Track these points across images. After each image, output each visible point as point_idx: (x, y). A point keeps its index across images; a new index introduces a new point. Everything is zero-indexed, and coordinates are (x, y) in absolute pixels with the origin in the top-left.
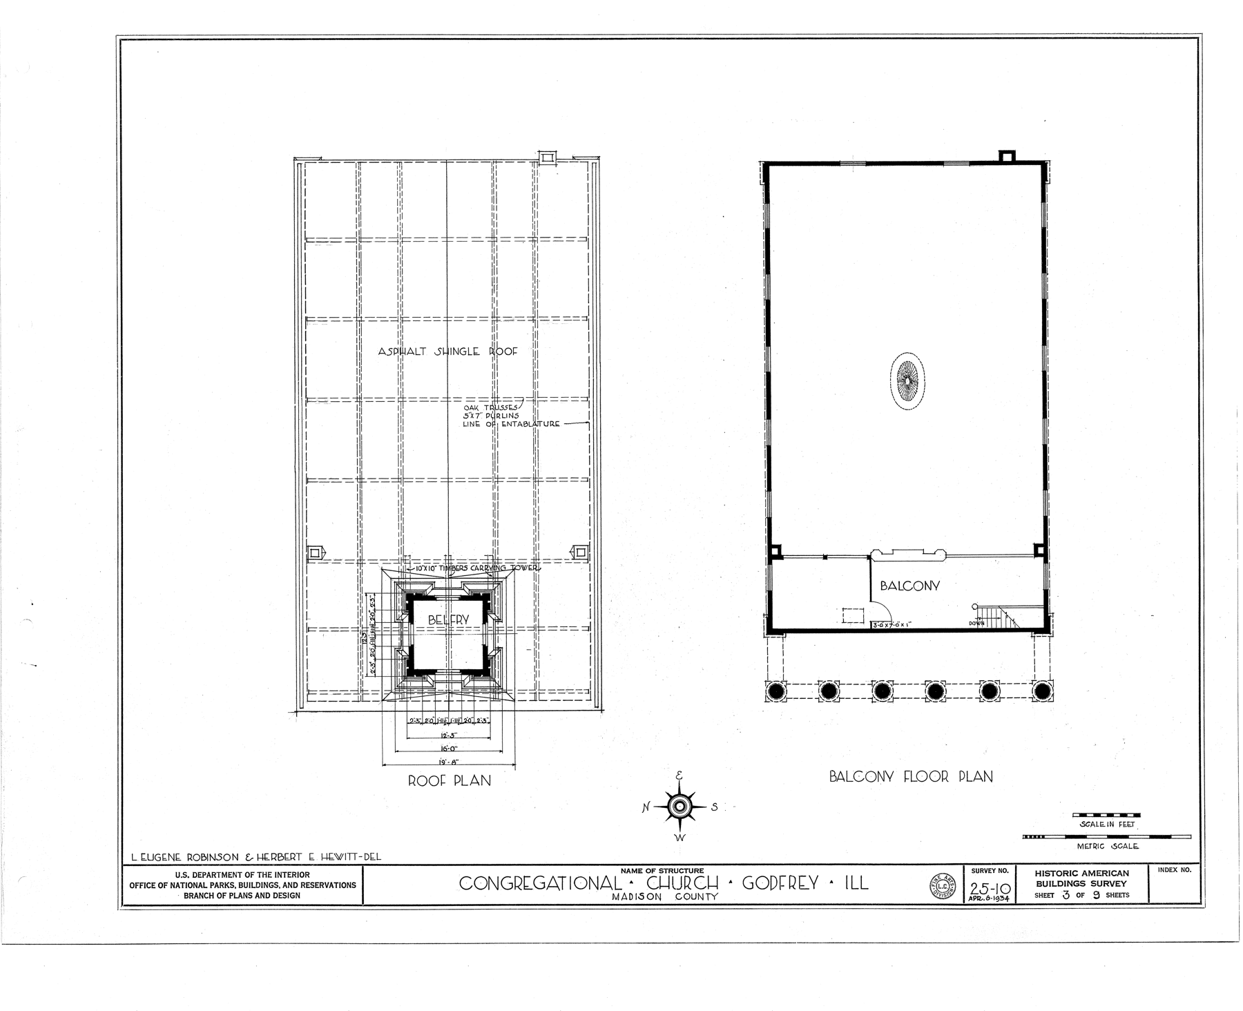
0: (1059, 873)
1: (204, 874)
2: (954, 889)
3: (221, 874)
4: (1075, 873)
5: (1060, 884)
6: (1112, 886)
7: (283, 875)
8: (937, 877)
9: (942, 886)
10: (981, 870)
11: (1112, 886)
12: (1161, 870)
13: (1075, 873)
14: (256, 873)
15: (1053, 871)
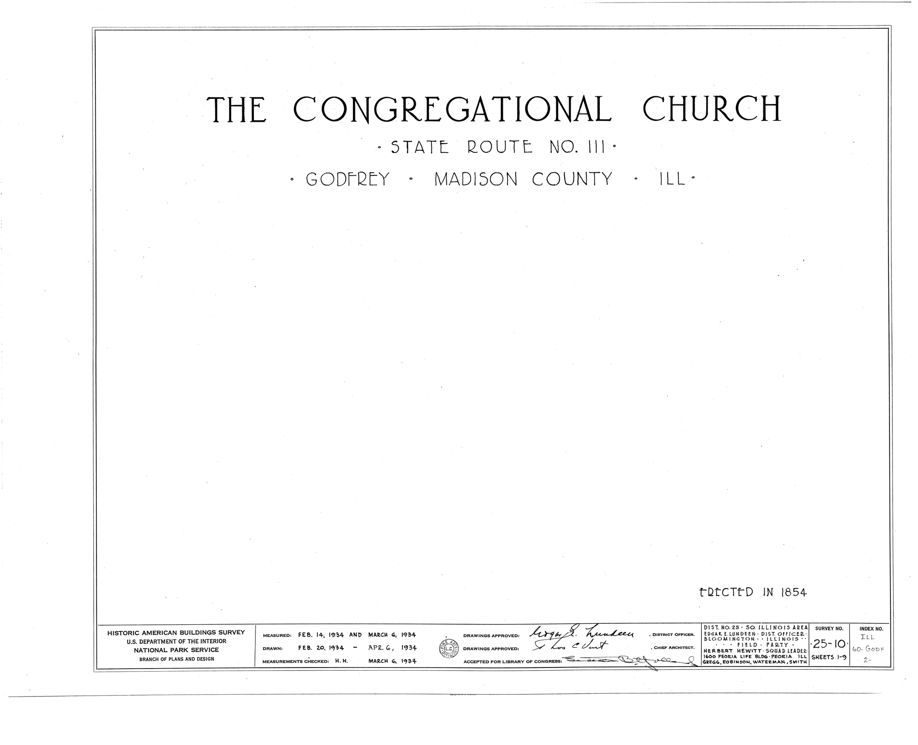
0: (125, 633)
1: (148, 641)
2: (457, 651)
3: (160, 641)
4: (137, 633)
5: (198, 632)
6: (234, 634)
7: (207, 641)
8: (444, 642)
9: (448, 648)
10: (823, 628)
11: (234, 634)
12: (817, 628)
13: (137, 633)
14: (187, 640)
15: (121, 632)
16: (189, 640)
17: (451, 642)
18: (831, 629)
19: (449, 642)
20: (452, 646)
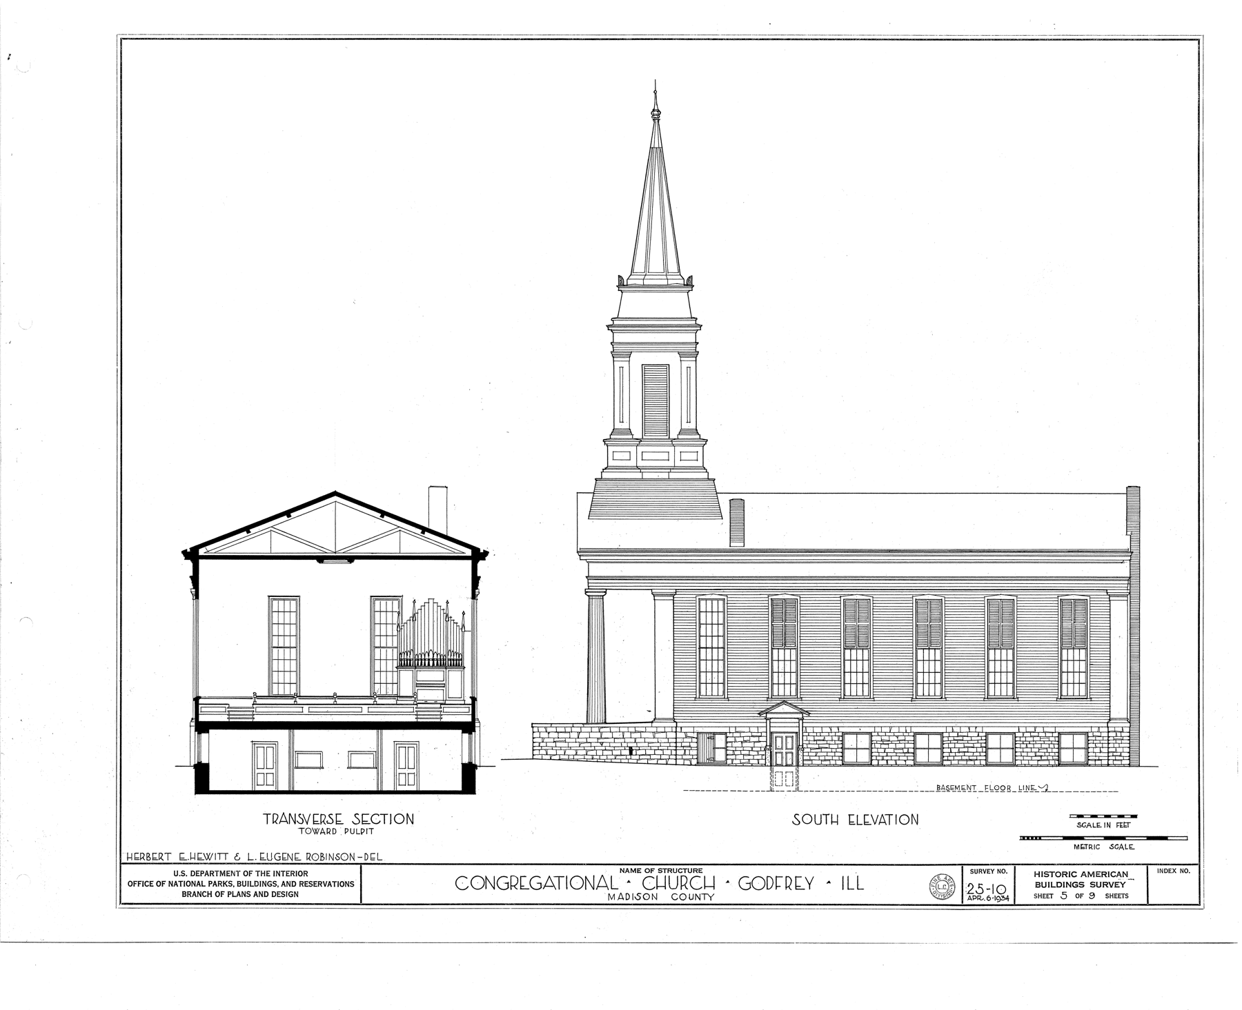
0: (1058, 874)
1: (202, 872)
2: (953, 890)
3: (219, 873)
4: (1074, 874)
6: (1111, 887)
7: (281, 873)
8: (936, 878)
9: (941, 887)
11: (1111, 887)
12: (1160, 871)
13: (1074, 874)
15: (1052, 872)
19: (942, 877)
20: (946, 883)
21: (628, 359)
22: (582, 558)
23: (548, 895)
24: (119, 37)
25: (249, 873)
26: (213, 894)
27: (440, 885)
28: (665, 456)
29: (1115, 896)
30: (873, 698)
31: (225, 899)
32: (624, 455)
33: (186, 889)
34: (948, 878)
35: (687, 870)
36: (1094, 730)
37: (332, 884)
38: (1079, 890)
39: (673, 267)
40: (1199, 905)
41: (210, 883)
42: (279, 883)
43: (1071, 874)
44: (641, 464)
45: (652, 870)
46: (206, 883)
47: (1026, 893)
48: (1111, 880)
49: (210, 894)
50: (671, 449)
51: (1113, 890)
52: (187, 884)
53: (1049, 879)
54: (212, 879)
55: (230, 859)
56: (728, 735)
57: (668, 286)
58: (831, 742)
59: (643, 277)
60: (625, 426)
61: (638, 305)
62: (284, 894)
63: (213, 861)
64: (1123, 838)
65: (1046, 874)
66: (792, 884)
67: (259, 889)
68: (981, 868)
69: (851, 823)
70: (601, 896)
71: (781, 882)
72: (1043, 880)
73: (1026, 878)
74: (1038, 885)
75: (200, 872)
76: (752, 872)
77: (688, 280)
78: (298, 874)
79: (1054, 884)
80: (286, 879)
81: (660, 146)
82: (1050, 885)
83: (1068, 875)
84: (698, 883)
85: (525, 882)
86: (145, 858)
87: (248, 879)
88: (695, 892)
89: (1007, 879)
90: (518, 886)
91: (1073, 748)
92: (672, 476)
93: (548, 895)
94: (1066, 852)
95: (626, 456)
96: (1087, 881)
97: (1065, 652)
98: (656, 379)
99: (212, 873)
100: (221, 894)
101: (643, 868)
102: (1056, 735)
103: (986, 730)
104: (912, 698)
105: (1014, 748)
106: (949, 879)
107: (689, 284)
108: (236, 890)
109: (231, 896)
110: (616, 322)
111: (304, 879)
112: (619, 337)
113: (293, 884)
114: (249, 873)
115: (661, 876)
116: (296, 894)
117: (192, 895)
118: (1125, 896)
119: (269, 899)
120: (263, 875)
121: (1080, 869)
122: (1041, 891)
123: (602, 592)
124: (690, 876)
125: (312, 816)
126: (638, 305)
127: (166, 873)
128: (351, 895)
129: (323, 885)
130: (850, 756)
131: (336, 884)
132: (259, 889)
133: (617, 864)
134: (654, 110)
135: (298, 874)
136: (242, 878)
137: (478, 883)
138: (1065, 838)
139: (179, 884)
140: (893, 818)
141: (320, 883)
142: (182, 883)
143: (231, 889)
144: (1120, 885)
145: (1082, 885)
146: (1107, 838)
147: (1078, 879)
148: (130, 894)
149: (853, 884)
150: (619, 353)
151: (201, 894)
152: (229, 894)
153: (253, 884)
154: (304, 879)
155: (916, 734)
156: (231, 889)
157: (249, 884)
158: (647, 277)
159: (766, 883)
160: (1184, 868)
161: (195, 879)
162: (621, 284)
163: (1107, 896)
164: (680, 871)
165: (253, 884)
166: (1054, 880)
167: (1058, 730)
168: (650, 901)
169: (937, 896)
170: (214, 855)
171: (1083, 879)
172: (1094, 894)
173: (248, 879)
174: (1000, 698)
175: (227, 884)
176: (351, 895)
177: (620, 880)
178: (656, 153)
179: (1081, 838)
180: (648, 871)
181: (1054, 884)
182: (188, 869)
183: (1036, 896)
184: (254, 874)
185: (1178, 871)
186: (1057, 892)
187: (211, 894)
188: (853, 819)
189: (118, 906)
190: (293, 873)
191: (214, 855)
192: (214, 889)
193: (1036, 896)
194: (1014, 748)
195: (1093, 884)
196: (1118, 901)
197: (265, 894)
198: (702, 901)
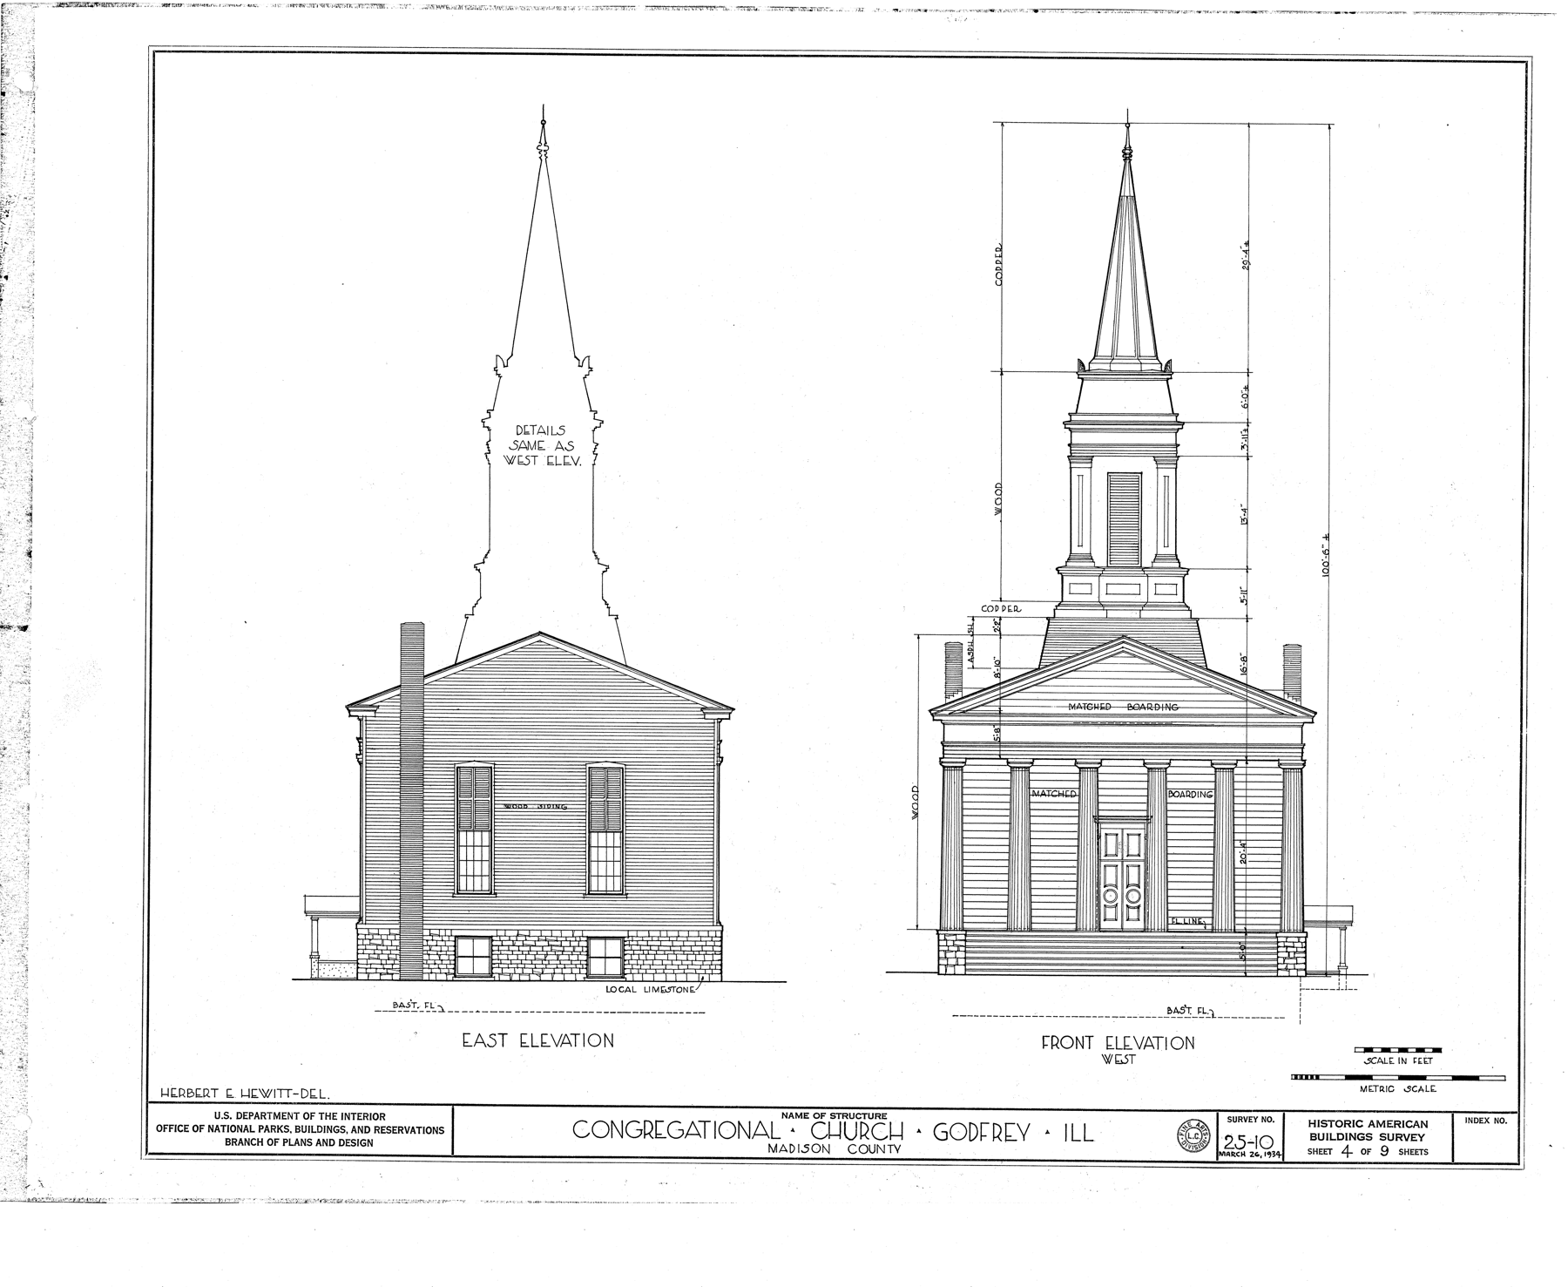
1: (251, 1114)
2: (1207, 1140)
3: (272, 1115)
4: (1359, 1124)
6: (1407, 1140)
8: (1186, 1124)
9: (1192, 1135)
11: (1407, 1140)
12: (1469, 1120)
13: (1359, 1124)
16: (322, 1113)
17: (1198, 1125)
18: (1253, 1120)
19: (1194, 1124)
20: (1198, 1132)
21: (1089, 465)
22: (352, 713)
23: (692, 1146)
24: (152, 49)
25: (311, 1116)
26: (265, 1142)
27: (553, 1132)
28: (1111, 589)
29: (1410, 1152)
30: (495, 894)
31: (279, 1148)
32: (1082, 588)
33: (231, 1135)
34: (1201, 1124)
35: (867, 1116)
36: (500, 933)
37: (417, 1130)
38: (1365, 1144)
39: (1147, 350)
40: (1519, 1164)
41: (261, 1127)
42: (349, 1129)
43: (1356, 1124)
44: (1104, 598)
45: (822, 1115)
46: (255, 1128)
47: (1298, 1147)
48: (1406, 1131)
49: (260, 1142)
50: (1143, 580)
51: (1409, 1145)
52: (230, 1129)
53: (1328, 1130)
54: (264, 1122)
55: (221, 1096)
56: (494, 938)
57: (1141, 373)
58: (639, 952)
59: (1109, 361)
60: (1085, 550)
61: (1103, 397)
62: (355, 1143)
63: (271, 1099)
64: (1423, 1078)
65: (1324, 1123)
66: (1000, 1134)
67: (322, 1136)
68: (1240, 1116)
69: (522, 1044)
70: (759, 1147)
71: (987, 1130)
72: (1320, 1130)
73: (1298, 1128)
74: (1313, 1137)
75: (248, 1114)
76: (950, 1117)
77: (1166, 365)
78: (372, 1117)
79: (1334, 1137)
80: (357, 1123)
81: (1132, 195)
82: (1329, 1137)
83: (1351, 1125)
84: (882, 1131)
85: (662, 1128)
86: (186, 1095)
87: (308, 1123)
88: (877, 1142)
89: (1274, 1129)
90: (653, 1134)
91: (473, 957)
92: (1145, 614)
93: (692, 1146)
94: (1351, 1095)
95: (1087, 589)
96: (1376, 1132)
97: (463, 835)
98: (1128, 493)
99: (263, 1115)
100: (275, 1142)
101: (812, 1112)
102: (452, 938)
103: (455, 933)
104: (454, 893)
105: (622, 957)
106: (1202, 1126)
107: (1167, 372)
108: (293, 1137)
109: (287, 1144)
110: (1074, 418)
111: (380, 1123)
112: (1079, 438)
113: (365, 1130)
114: (311, 1116)
115: (835, 1123)
116: (370, 1143)
117: (237, 1143)
118: (1423, 1152)
119: (336, 1149)
120: (328, 1118)
121: (1367, 1118)
122: (1317, 1144)
123: (1163, 764)
124: (871, 1123)
125: (1114, 1057)
126: (1103, 397)
127: (204, 1115)
128: (440, 1144)
129: (404, 1130)
130: (464, 966)
131: (421, 1130)
132: (322, 1136)
133: (333, 1104)
134: (1125, 148)
135: (372, 1117)
136: (301, 1122)
137: (601, 1129)
138: (1348, 1077)
139: (221, 1128)
140: (580, 1038)
141: (401, 1129)
142: (226, 1128)
143: (287, 1136)
144: (1418, 1138)
145: (1369, 1137)
146: (1402, 1078)
147: (1365, 1130)
148: (159, 1142)
149: (1079, 1135)
150: (1078, 456)
151: (249, 1142)
152: (284, 1143)
153: (315, 1129)
154: (380, 1123)
155: (589, 938)
156: (287, 1136)
157: (310, 1129)
158: (1114, 361)
159: (968, 1132)
160: (172, 1097)
161: (242, 1122)
162: (1082, 370)
163: (1402, 1152)
164: (859, 1116)
165: (315, 1129)
166: (1334, 1131)
167: (586, 934)
168: (820, 1155)
169: (1187, 1148)
170: (273, 1092)
171: (1371, 1130)
172: (1387, 1150)
173: (308, 1123)
174: (474, 893)
175: (283, 1129)
176: (440, 1144)
177: (782, 1127)
178: (1127, 204)
179: (1369, 1077)
180: (817, 1116)
181: (1334, 1137)
182: (233, 1110)
183: (1311, 1151)
184: (317, 1116)
185: (1491, 1120)
186: (1338, 1146)
187: (262, 1142)
188: (527, 1039)
189: (144, 1157)
190: (366, 1116)
191: (273, 1092)
192: (265, 1136)
193: (1311, 1151)
194: (456, 956)
195: (1383, 1137)
196: (1416, 1160)
197: (330, 1143)
198: (887, 1155)
